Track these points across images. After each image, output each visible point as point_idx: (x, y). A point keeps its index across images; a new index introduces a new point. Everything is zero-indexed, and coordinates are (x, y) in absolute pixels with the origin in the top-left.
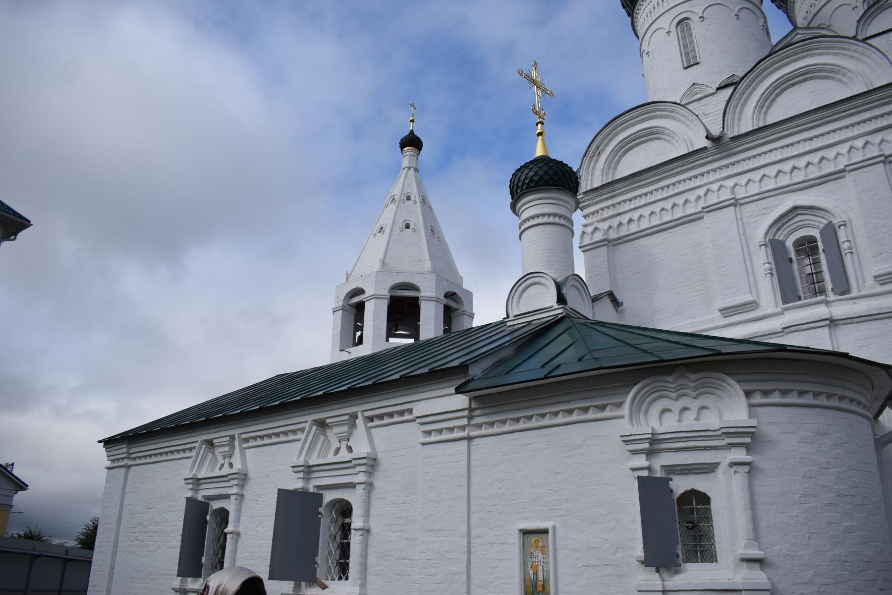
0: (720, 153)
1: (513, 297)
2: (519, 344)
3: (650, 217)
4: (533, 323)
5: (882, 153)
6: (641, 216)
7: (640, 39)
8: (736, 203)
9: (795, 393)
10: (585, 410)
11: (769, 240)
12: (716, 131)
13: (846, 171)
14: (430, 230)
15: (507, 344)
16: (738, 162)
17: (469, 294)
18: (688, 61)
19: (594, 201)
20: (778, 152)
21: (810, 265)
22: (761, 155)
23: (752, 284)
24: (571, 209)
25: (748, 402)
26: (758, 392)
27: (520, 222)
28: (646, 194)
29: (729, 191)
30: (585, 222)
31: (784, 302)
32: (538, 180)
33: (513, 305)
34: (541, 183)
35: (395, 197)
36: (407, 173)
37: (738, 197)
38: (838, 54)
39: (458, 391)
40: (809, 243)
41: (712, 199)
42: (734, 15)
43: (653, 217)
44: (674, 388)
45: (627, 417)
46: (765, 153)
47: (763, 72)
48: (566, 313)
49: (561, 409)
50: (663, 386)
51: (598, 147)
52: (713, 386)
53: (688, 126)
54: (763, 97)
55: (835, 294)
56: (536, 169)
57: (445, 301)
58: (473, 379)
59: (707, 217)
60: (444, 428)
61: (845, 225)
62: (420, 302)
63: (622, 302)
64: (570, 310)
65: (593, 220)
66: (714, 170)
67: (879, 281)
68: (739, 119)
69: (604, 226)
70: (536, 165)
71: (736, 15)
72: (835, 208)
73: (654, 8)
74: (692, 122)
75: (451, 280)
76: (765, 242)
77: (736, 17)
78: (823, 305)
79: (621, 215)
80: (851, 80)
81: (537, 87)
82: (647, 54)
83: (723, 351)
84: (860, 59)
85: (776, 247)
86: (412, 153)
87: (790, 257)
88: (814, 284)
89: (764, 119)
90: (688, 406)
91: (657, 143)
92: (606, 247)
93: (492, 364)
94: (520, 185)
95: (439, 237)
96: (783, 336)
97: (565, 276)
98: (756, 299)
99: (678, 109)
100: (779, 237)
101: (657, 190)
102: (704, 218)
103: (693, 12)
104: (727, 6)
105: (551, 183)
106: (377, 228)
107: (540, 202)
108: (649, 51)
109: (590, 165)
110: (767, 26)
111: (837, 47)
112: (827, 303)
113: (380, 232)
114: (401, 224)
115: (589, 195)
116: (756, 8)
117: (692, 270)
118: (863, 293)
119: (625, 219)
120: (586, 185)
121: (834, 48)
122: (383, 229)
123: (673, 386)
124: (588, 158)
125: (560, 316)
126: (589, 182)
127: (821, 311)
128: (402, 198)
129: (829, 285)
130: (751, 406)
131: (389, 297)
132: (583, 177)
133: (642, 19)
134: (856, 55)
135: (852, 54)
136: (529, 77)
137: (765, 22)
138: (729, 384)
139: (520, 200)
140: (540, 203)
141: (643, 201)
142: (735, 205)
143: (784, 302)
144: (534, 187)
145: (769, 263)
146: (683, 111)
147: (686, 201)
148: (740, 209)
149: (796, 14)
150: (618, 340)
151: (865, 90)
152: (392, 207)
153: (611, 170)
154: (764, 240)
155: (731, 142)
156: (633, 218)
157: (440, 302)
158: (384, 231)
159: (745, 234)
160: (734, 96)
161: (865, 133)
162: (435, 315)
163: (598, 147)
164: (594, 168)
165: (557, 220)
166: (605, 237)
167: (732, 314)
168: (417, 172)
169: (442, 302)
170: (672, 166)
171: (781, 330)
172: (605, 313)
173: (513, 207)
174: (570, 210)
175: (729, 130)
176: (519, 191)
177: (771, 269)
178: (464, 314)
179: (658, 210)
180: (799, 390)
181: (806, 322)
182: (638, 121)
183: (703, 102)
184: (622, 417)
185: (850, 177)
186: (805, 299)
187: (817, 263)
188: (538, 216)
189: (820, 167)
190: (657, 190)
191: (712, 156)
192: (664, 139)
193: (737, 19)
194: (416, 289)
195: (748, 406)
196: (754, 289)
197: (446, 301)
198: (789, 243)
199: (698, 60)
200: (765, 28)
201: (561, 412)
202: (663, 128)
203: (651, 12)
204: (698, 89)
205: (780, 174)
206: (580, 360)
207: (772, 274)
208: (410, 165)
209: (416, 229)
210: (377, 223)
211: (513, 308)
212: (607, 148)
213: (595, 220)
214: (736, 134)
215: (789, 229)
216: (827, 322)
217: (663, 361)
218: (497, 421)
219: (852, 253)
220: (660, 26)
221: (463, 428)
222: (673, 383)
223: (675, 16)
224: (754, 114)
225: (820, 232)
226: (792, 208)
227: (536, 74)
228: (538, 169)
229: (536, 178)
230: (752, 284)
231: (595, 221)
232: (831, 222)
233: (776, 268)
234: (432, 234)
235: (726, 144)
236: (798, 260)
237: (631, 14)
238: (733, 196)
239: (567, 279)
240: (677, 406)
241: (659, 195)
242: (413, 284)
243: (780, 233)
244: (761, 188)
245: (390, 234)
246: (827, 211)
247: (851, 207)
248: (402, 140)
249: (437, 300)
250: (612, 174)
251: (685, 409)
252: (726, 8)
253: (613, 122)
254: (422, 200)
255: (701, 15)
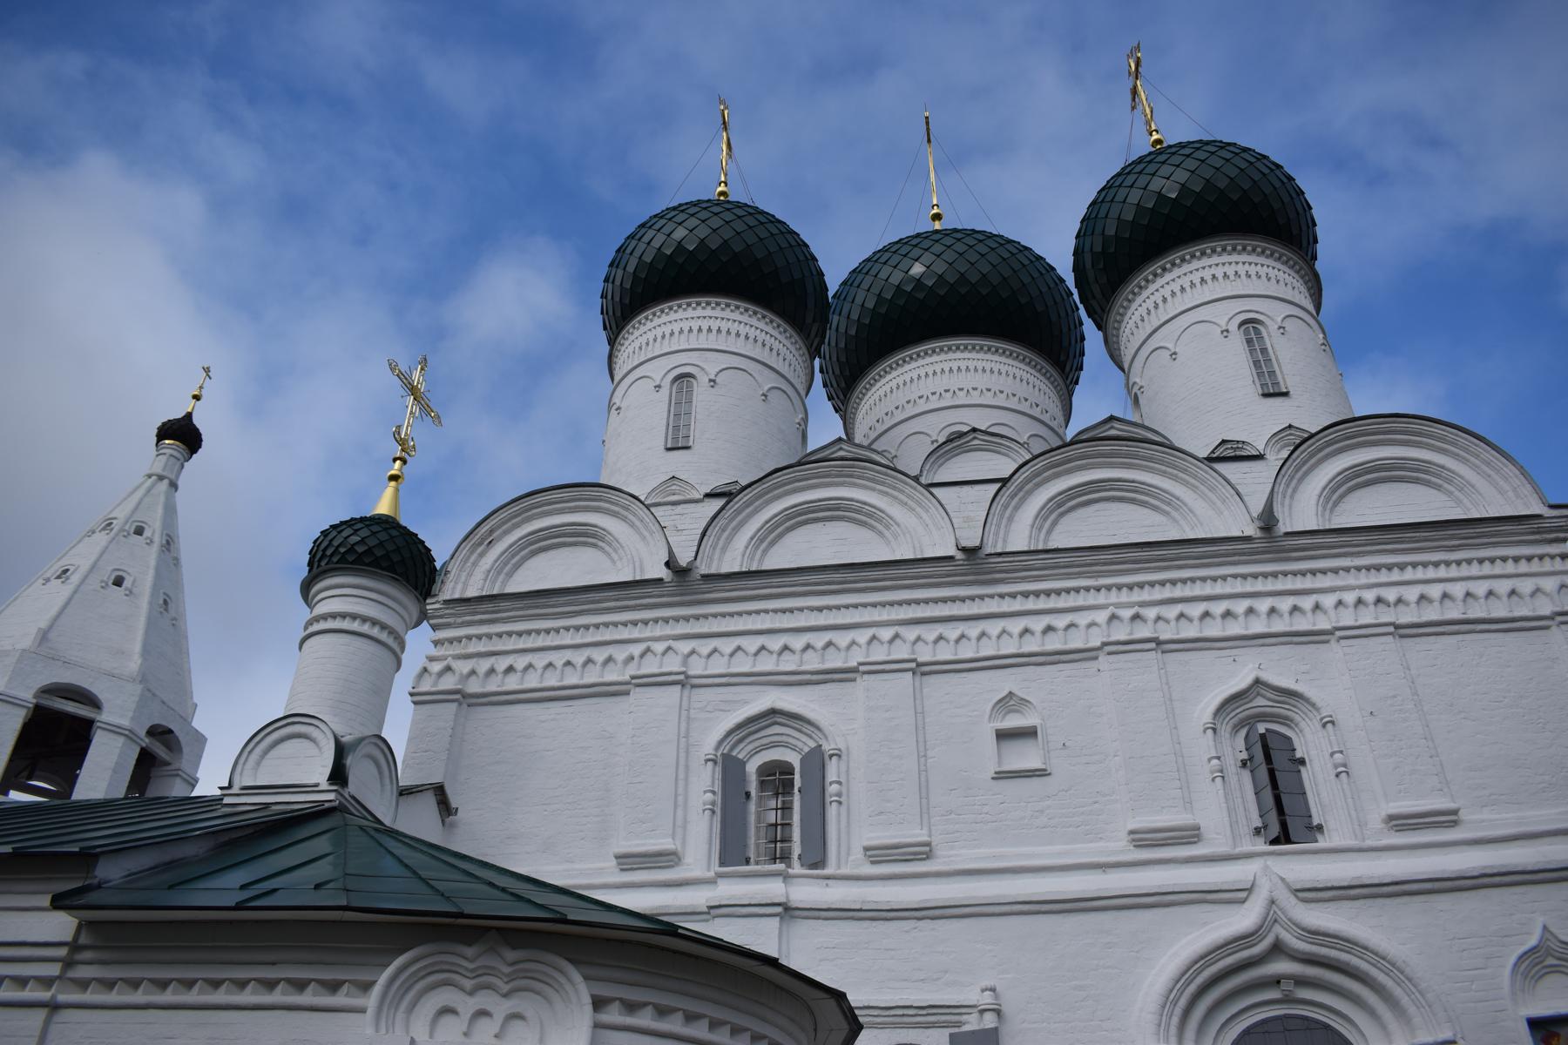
0: (681, 595)
1: (250, 752)
2: (225, 838)
3: (544, 672)
4: (274, 807)
5: (913, 657)
6: (530, 666)
7: (615, 382)
8: (685, 682)
9: (680, 1015)
10: (300, 985)
11: (723, 754)
12: (684, 559)
13: (859, 671)
14: (161, 602)
15: (198, 833)
16: (706, 617)
17: (200, 740)
18: (675, 439)
19: (459, 620)
20: (768, 617)
21: (777, 809)
22: (741, 615)
23: (679, 822)
24: (408, 620)
25: (594, 1017)
26: (617, 1002)
27: (310, 617)
28: (548, 631)
29: (679, 659)
30: (434, 652)
31: (722, 864)
32: (362, 553)
33: (246, 767)
34: (367, 560)
35: (115, 522)
36: (153, 486)
37: (691, 673)
38: (886, 494)
39: (59, 903)
40: (781, 774)
41: (650, 666)
42: (761, 392)
43: (549, 673)
44: (472, 971)
45: (370, 1012)
46: (749, 613)
47: (776, 489)
48: (340, 802)
49: (254, 976)
50: (447, 963)
51: (491, 531)
52: (540, 978)
53: (644, 538)
54: (767, 526)
55: (802, 865)
56: (365, 533)
57: (146, 741)
58: (99, 886)
59: (638, 694)
60: (7, 977)
61: (839, 756)
62: (94, 729)
63: (457, 809)
64: (350, 799)
65: (447, 653)
66: (666, 620)
67: (870, 856)
68: (724, 550)
69: (463, 667)
70: (367, 526)
71: (763, 395)
72: (832, 726)
73: (647, 344)
74: (652, 533)
75: (171, 705)
76: (716, 756)
77: (763, 397)
78: (780, 879)
79: (498, 657)
80: (896, 537)
81: (415, 399)
82: (617, 410)
83: (571, 917)
84: (914, 510)
85: (730, 768)
86: (175, 453)
87: (747, 790)
88: (776, 842)
89: (761, 560)
90: (489, 1008)
91: (590, 551)
92: (455, 704)
93: (152, 865)
94: (329, 552)
95: (175, 619)
96: (707, 921)
97: (360, 735)
98: (679, 849)
99: (636, 506)
100: (739, 753)
101: (567, 629)
102: (631, 693)
103: (703, 369)
104: (754, 378)
105: (384, 564)
106: (57, 568)
107: (355, 592)
108: (622, 406)
109: (469, 557)
110: (806, 428)
111: (888, 484)
112: (786, 877)
113: (59, 577)
114: (107, 576)
115: (452, 608)
116: (796, 394)
117: (588, 778)
118: (844, 871)
119: (502, 664)
120: (454, 588)
121: (883, 484)
122: (68, 574)
123: (471, 966)
124: (470, 545)
125: (327, 805)
126: (460, 586)
127: (773, 889)
128: (127, 528)
129: (797, 850)
130: (597, 1026)
131: (31, 705)
132: (453, 574)
133: (625, 355)
134: (909, 502)
135: (906, 499)
136: (406, 379)
137: (805, 420)
138: (570, 980)
139: (321, 580)
140: (355, 593)
141: (540, 641)
142: (682, 684)
143: (722, 864)
144: (351, 563)
145: (714, 793)
146: (641, 512)
147: (609, 660)
148: (690, 693)
149: (857, 426)
150: (406, 866)
151: (912, 557)
152: (101, 539)
153: (502, 576)
154: (713, 752)
155: (701, 582)
156: (515, 665)
157: (134, 741)
158: (67, 579)
159: (687, 736)
160: (724, 511)
161: (898, 620)
162: (116, 763)
163: (491, 531)
164: (475, 564)
165: (375, 632)
166: (460, 687)
167: (635, 866)
168: (174, 490)
169: (139, 741)
170: (606, 594)
171: (706, 910)
172: (420, 822)
173: (306, 588)
174: (404, 621)
175: (704, 564)
176: (323, 563)
177: (713, 803)
178: (178, 775)
179: (559, 663)
180: (688, 1011)
181: (747, 903)
182: (570, 508)
183: (679, 509)
184: (363, 1011)
185: (863, 682)
186: (757, 863)
187: (786, 808)
188: (343, 616)
189: (823, 655)
190: (567, 629)
191: (669, 596)
192: (602, 549)
193: (764, 400)
194: (94, 703)
195: (592, 1025)
196: (679, 831)
197: (147, 740)
198: (752, 767)
199: (691, 444)
200: (801, 428)
201: (253, 982)
202: (604, 530)
203: (640, 348)
204: (678, 488)
205: (764, 652)
206: (318, 887)
207: (713, 812)
208: (165, 474)
209: (134, 590)
210: (59, 560)
211: (245, 772)
212: (507, 537)
213: (451, 653)
214: (713, 571)
215: (757, 744)
216: (779, 909)
217: (461, 915)
218: (121, 979)
219: (840, 803)
220: (648, 374)
221: (47, 982)
222: (471, 961)
223: (674, 365)
224: (747, 547)
225: (801, 759)
226: (768, 710)
227: (419, 377)
228: (368, 533)
229: (360, 549)
230: (679, 822)
231: (450, 655)
232: (821, 746)
233: (722, 803)
234: (162, 610)
235: (692, 583)
236: (760, 798)
237: (612, 342)
238: (683, 669)
239: (360, 740)
240: (467, 1005)
241: (567, 638)
242: (79, 687)
243: (741, 746)
244: (729, 668)
245: (79, 586)
246: (818, 728)
247: (853, 729)
248: (164, 424)
249: (130, 735)
250: (502, 583)
251: (483, 1013)
252: (752, 379)
253: (528, 498)
254: (164, 542)
255: (713, 377)
